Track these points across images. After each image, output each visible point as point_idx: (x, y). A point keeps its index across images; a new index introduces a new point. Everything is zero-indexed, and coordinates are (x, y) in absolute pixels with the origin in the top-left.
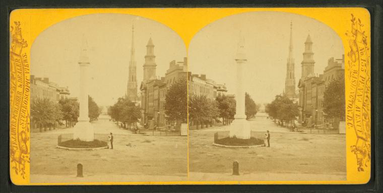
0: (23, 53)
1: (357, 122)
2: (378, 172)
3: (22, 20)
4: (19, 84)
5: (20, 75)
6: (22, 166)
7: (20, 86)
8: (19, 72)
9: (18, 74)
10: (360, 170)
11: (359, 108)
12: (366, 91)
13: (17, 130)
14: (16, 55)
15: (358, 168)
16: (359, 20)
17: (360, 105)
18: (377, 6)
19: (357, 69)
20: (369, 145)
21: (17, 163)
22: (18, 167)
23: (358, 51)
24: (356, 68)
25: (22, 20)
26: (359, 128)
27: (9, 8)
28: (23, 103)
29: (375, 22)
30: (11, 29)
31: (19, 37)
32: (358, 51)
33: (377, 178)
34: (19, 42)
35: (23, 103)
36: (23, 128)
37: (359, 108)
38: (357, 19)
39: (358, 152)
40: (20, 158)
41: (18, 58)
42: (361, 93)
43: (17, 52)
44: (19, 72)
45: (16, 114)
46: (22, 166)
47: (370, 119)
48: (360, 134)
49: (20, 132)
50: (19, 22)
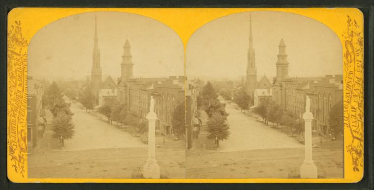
0: (23, 52)
1: (353, 122)
2: (371, 171)
3: (23, 20)
4: (18, 82)
5: (20, 74)
6: (21, 165)
7: (20, 85)
8: (18, 71)
9: (18, 72)
10: (19, 22)
11: (355, 109)
12: (12, 101)
13: (16, 128)
14: (358, 138)
15: (354, 169)
16: (355, 21)
17: (356, 105)
18: (371, 7)
19: (353, 70)
20: (9, 48)
21: (16, 161)
22: (17, 165)
23: (353, 52)
24: (352, 69)
25: (23, 20)
26: (354, 128)
27: (7, 7)
28: (23, 102)
29: (370, 23)
30: (363, 164)
31: (19, 36)
32: (353, 52)
33: (371, 177)
34: (19, 42)
35: (23, 102)
36: (22, 126)
37: (355, 109)
38: (353, 21)
39: (20, 40)
40: (352, 36)
41: (18, 57)
42: (357, 94)
43: (17, 51)
44: (18, 71)
45: (15, 113)
46: (21, 165)
47: (8, 73)
48: (355, 134)
49: (19, 130)
50: (20, 22)
